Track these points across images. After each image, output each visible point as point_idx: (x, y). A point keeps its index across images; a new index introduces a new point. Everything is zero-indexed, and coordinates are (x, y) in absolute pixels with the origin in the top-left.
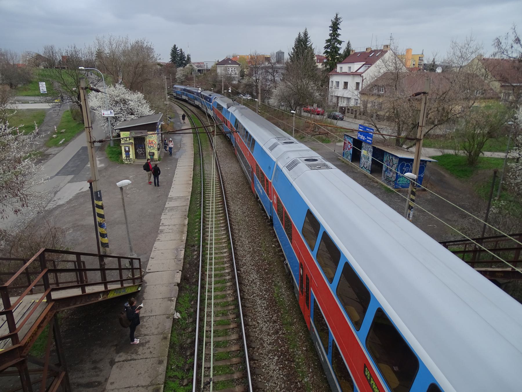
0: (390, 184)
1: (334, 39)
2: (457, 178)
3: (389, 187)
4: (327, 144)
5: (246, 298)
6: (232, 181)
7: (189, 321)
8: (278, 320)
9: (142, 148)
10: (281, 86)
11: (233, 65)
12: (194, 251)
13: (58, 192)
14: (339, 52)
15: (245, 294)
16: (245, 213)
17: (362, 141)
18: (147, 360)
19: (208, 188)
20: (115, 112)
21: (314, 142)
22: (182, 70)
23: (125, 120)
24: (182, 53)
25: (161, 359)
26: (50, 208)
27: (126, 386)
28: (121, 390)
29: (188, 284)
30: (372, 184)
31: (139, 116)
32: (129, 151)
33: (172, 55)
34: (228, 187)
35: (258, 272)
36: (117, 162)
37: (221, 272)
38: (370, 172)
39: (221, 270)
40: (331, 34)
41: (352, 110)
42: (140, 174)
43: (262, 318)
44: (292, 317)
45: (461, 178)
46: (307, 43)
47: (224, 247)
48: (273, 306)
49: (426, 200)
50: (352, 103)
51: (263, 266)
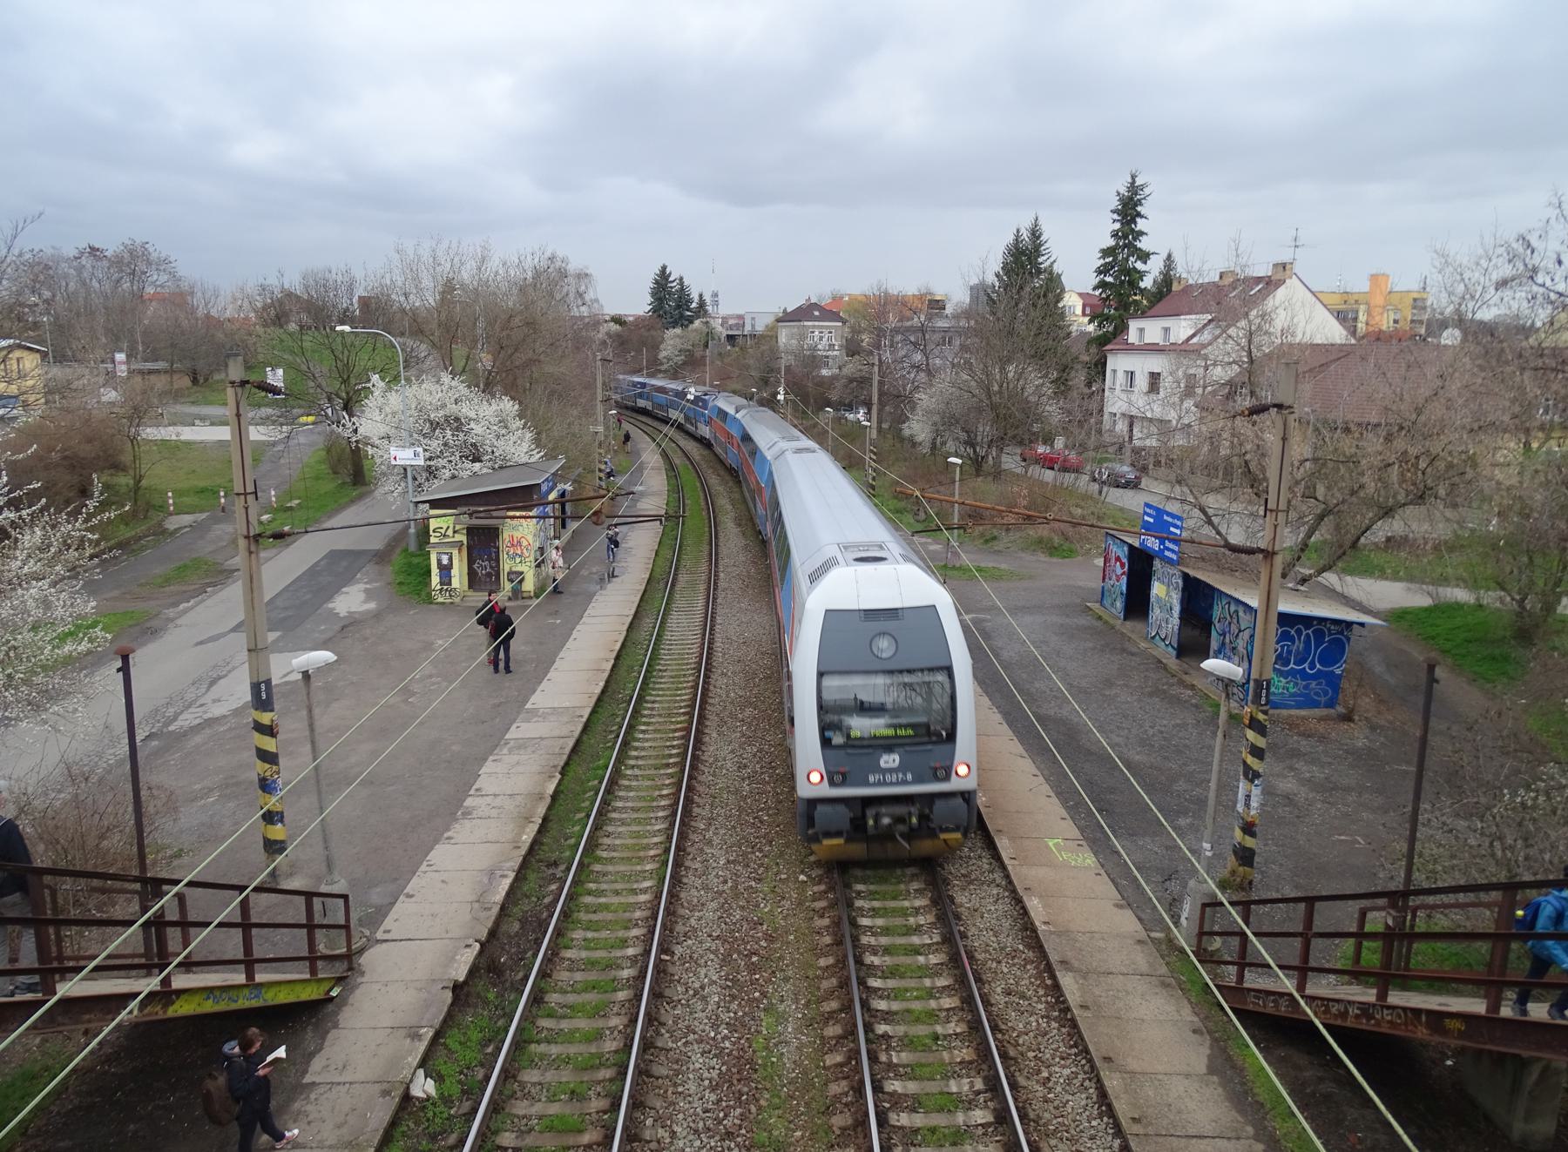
1: (1125, 246)
2: (1474, 680)
4: (1067, 560)
5: (659, 1044)
6: (738, 668)
7: (459, 1108)
8: (741, 1129)
9: (490, 560)
10: (944, 383)
12: (553, 879)
13: (222, 681)
14: (1142, 285)
15: (663, 1031)
16: (745, 766)
17: (1151, 553)
19: (657, 686)
20: (428, 454)
21: (1023, 555)
22: (678, 336)
23: (454, 477)
24: (682, 289)
26: (182, 727)
29: (495, 986)
30: (1175, 690)
31: (496, 466)
32: (449, 567)
33: (653, 295)
34: (719, 683)
35: (726, 960)
36: (416, 597)
37: (612, 955)
38: (1175, 652)
39: (612, 947)
40: (1118, 231)
43: (690, 1119)
44: (790, 1122)
47: (647, 874)
48: (739, 1080)
49: (1347, 752)
51: (748, 942)
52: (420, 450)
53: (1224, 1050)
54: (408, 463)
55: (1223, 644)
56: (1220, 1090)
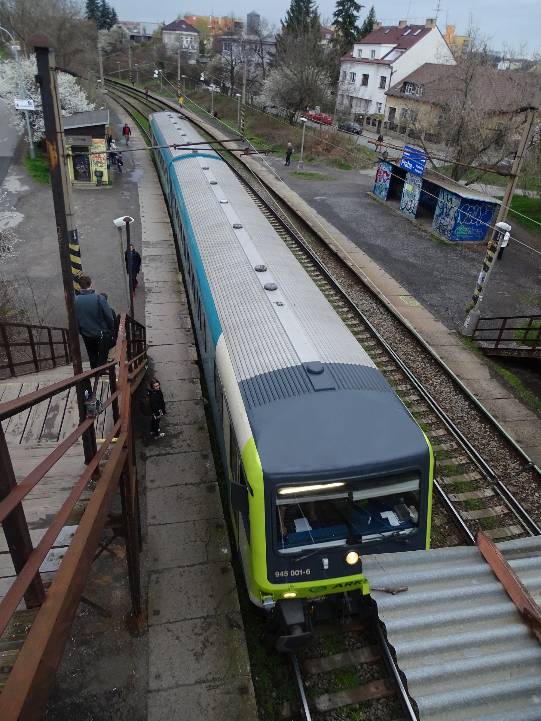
0: (445, 234)
3: (443, 238)
9: (85, 164)
11: (189, 33)
18: (188, 454)
20: (36, 103)
25: (204, 453)
27: (172, 484)
28: (166, 488)
30: (419, 233)
31: (73, 112)
33: (87, 7)
38: (414, 216)
41: (375, 120)
42: (88, 205)
45: (532, 229)
46: (311, 5)
50: (372, 110)
52: (31, 101)
53: (493, 370)
54: (25, 108)
55: (442, 213)
56: (497, 383)
